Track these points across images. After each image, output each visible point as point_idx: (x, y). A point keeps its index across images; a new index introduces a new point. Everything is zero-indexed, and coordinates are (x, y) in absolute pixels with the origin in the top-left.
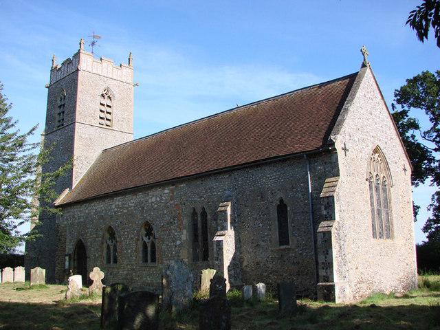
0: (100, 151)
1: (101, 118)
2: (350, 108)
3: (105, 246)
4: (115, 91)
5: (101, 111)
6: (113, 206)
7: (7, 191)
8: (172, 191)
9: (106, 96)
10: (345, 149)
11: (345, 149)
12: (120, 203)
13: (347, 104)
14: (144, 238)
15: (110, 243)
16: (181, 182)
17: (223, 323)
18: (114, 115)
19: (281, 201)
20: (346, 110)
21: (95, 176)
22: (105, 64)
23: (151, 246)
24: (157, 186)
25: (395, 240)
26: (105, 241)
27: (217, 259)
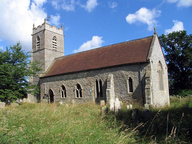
0: (54, 58)
1: (53, 47)
2: (153, 48)
3: (76, 91)
4: (58, 37)
5: (53, 45)
6: (64, 78)
7: (5, 68)
8: (88, 74)
9: (54, 39)
10: (152, 62)
11: (152, 62)
12: (66, 77)
13: (151, 47)
14: (77, 89)
15: (63, 91)
16: (91, 71)
17: (159, 6)
18: (57, 46)
19: (130, 78)
20: (152, 49)
21: (53, 68)
22: (53, 28)
23: (80, 92)
24: (82, 72)
25: (28, 99)
26: (75, 89)
27: (172, 89)
